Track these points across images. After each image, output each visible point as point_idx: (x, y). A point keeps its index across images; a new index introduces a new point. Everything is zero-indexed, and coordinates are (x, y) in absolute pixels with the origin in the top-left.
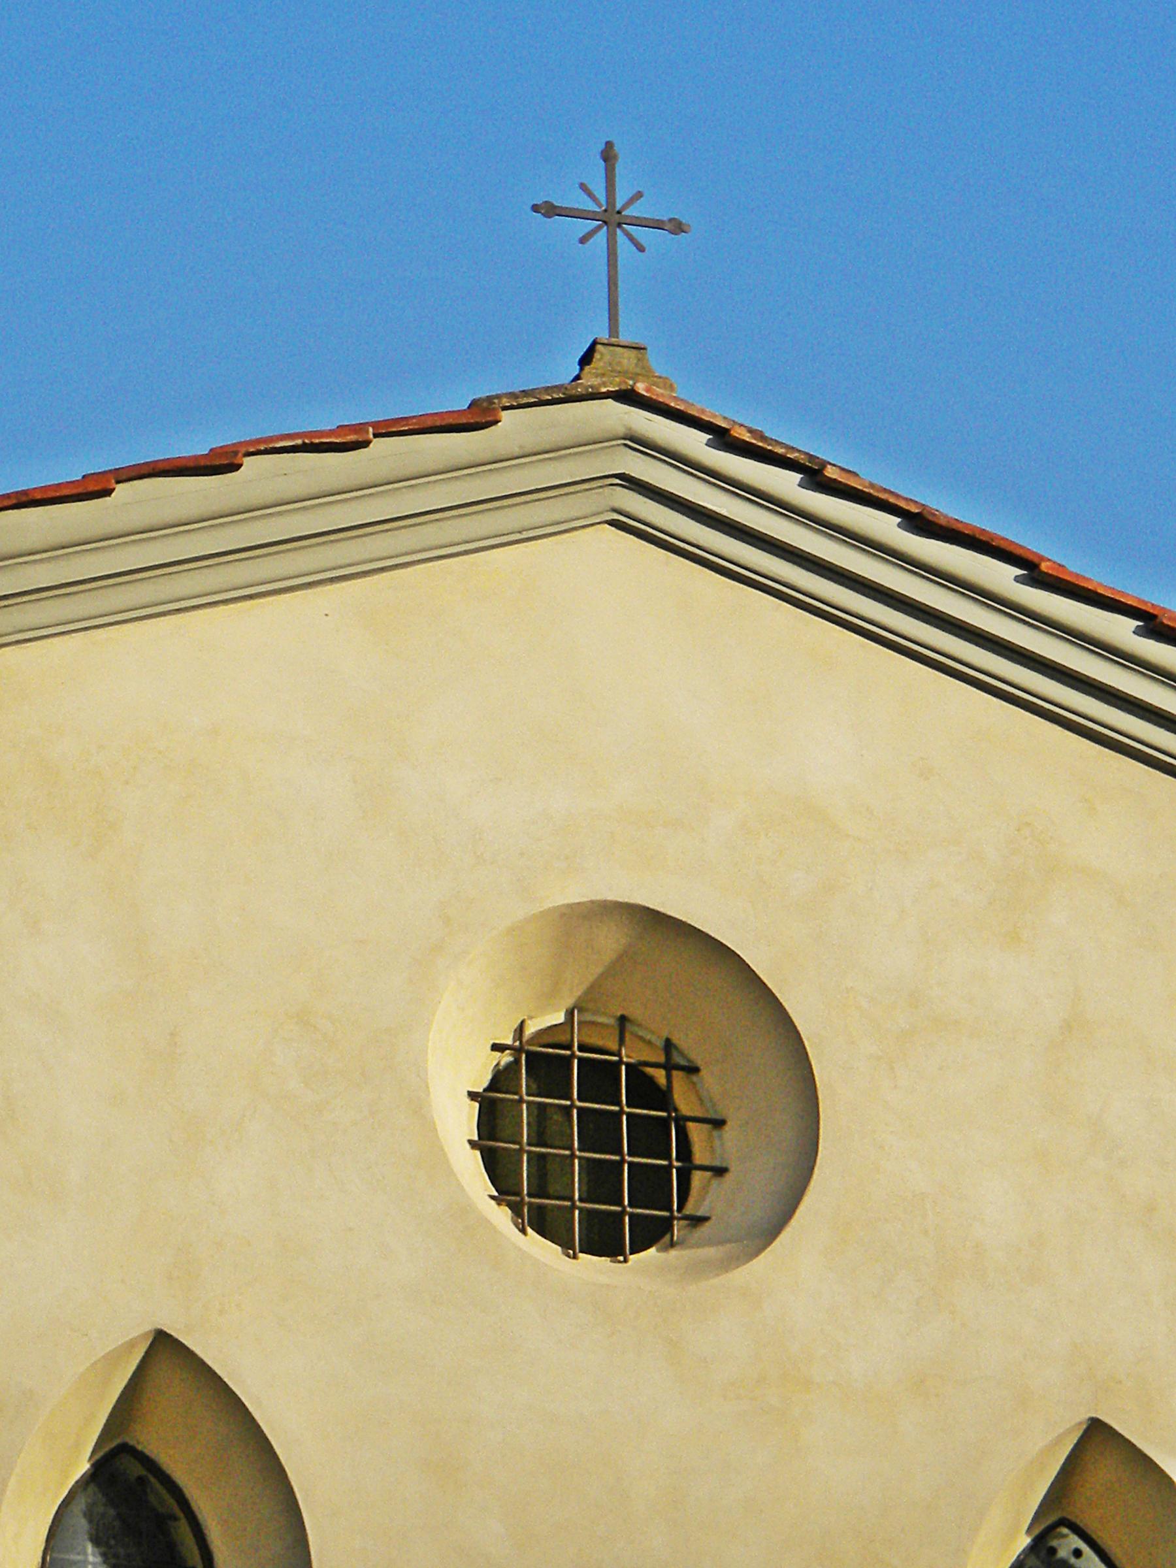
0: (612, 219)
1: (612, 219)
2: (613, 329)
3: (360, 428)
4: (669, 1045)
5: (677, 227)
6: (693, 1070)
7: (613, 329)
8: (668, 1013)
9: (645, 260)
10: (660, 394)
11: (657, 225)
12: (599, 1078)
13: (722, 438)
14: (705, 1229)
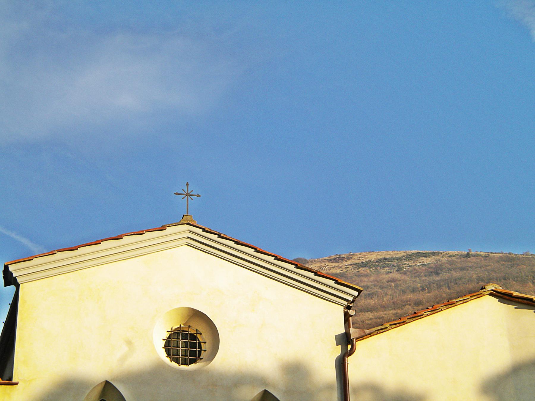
0: (188, 195)
1: (188, 195)
2: (187, 214)
3: (143, 231)
4: (197, 330)
5: (199, 196)
6: (201, 334)
7: (187, 214)
8: (197, 326)
9: (194, 202)
10: (194, 223)
11: (195, 196)
12: (185, 336)
13: (204, 230)
14: (202, 360)
